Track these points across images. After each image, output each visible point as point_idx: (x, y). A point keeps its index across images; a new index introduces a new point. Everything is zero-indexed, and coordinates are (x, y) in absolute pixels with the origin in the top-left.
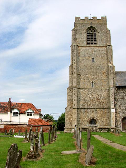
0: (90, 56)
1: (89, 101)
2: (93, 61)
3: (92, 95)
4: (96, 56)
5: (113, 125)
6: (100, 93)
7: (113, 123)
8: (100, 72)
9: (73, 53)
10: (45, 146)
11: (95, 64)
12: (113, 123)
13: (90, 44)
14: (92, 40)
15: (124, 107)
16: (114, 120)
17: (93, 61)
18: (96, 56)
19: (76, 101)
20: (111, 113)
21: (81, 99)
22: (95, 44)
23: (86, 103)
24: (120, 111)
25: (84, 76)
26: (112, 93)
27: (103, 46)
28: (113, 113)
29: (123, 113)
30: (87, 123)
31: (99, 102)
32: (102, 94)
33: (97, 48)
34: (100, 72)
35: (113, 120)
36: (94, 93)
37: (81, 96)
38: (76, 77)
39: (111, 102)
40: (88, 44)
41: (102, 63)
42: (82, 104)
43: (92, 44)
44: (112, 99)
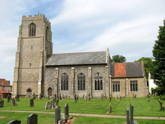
1: (27, 77)
2: (32, 49)
17: (32, 49)
28: (39, 85)
29: (49, 85)
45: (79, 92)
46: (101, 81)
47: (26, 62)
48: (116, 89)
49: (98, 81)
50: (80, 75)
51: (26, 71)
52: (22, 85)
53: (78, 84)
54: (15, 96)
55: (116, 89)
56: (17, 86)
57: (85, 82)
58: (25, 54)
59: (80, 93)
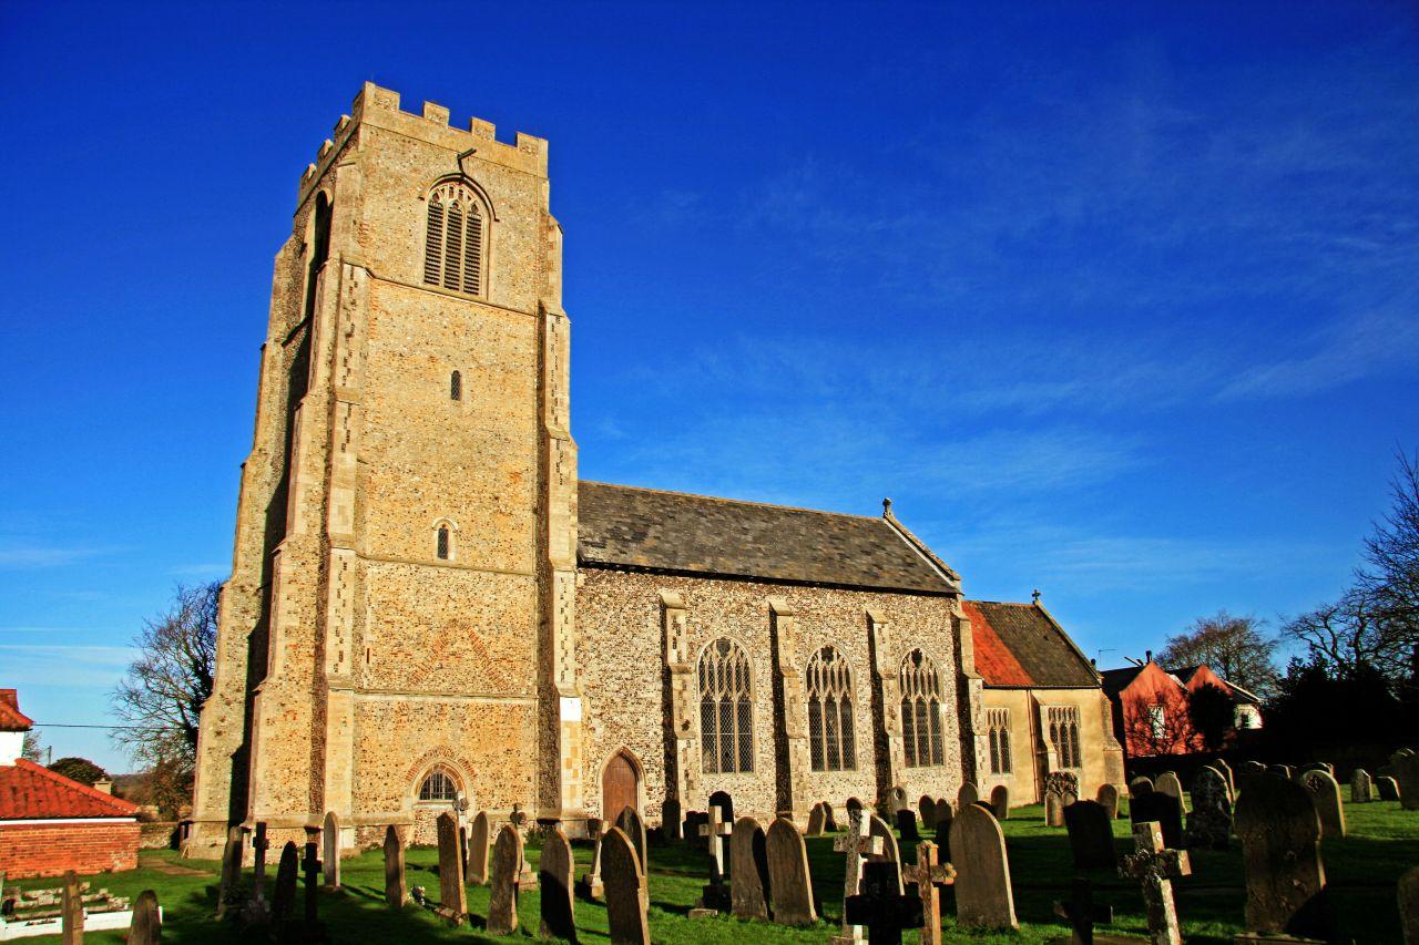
0: (438, 356)
1: (421, 644)
2: (456, 393)
3: (442, 606)
4: (474, 359)
5: (573, 795)
6: (486, 600)
7: (573, 787)
8: (493, 464)
9: (343, 316)
10: (852, 796)
11: (466, 409)
12: (573, 787)
13: (442, 282)
14: (453, 260)
15: (617, 688)
16: (576, 771)
17: (456, 393)
18: (474, 359)
19: (348, 639)
20: (562, 725)
21: (368, 628)
22: (472, 288)
23: (401, 656)
24: (598, 711)
25: (397, 479)
26: (563, 602)
27: (516, 307)
28: (569, 724)
29: (614, 727)
30: (331, 810)
31: (480, 651)
32: (501, 607)
33: (483, 316)
34: (493, 464)
35: (569, 766)
36: (454, 595)
37: (369, 610)
38: (352, 477)
39: (557, 659)
40: (430, 278)
41: (503, 411)
42: (372, 659)
43: (452, 283)
44: (562, 637)
45: (821, 779)
46: (934, 702)
47: (406, 503)
48: (923, 750)
49: (920, 701)
50: (820, 664)
51: (408, 596)
52: (1272, 662)
53: (815, 727)
54: (343, 162)
55: (923, 750)
56: (1047, 760)
57: (848, 712)
58: (392, 432)
59: (829, 789)
